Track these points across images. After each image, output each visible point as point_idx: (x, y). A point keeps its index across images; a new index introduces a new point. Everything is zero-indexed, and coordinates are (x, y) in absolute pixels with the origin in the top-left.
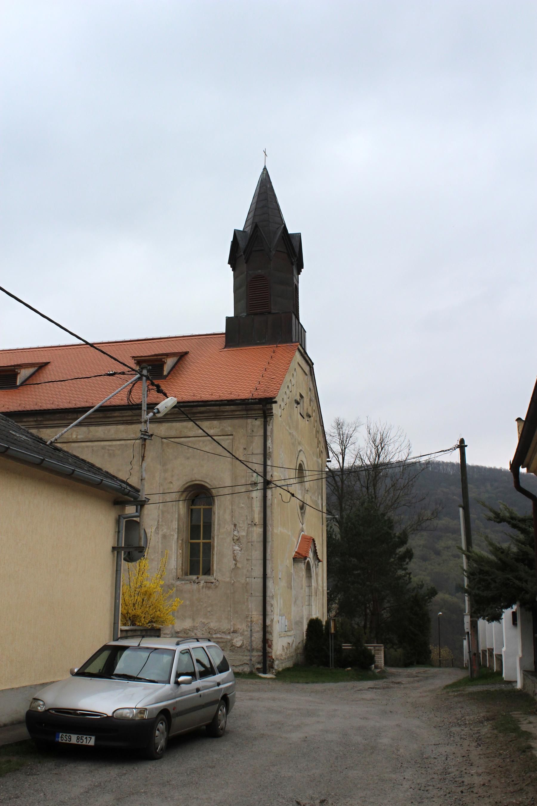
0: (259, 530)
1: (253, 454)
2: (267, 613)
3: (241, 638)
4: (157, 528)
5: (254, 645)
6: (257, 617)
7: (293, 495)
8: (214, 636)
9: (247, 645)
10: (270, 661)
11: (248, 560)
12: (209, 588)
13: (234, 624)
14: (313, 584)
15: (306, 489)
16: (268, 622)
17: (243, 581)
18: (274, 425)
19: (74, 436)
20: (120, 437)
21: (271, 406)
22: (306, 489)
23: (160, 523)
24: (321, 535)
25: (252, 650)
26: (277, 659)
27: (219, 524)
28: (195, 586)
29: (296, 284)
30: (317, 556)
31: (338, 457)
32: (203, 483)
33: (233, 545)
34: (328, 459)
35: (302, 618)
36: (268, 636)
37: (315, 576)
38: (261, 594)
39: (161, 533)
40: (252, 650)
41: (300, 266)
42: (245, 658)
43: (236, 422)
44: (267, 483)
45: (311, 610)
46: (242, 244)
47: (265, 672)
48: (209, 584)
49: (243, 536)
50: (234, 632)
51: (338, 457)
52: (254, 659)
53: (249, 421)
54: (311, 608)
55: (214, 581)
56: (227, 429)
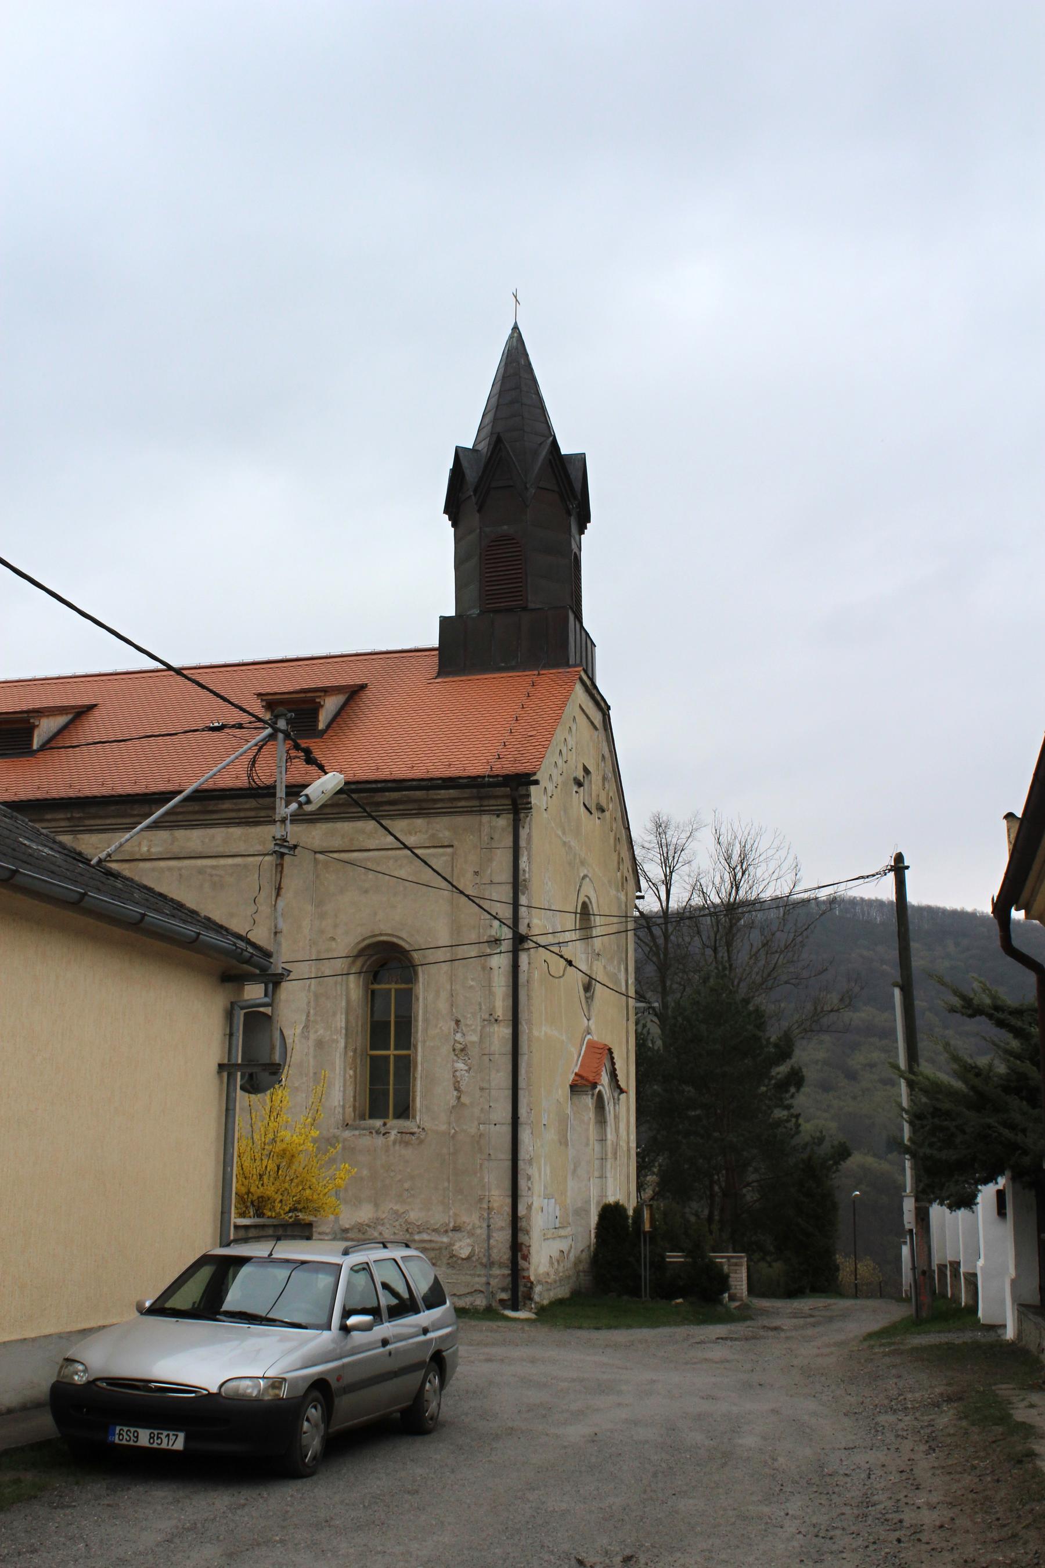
0: (504, 1031)
1: (492, 883)
2: (519, 1192)
3: (468, 1241)
4: (306, 1027)
5: (495, 1255)
6: (500, 1199)
7: (570, 963)
8: (417, 1237)
9: (481, 1255)
10: (525, 1286)
11: (482, 1089)
12: (407, 1144)
13: (455, 1214)
14: (609, 1137)
15: (596, 952)
16: (522, 1211)
17: (473, 1131)
18: (534, 826)
19: (145, 849)
20: (234, 850)
21: (528, 790)
22: (596, 952)
23: (312, 1018)
24: (624, 1040)
25: (491, 1264)
26: (539, 1282)
27: (426, 1020)
28: (380, 1140)
29: (575, 553)
30: (617, 1081)
31: (657, 889)
32: (395, 940)
33: (453, 1061)
34: (638, 894)
35: (588, 1202)
36: (522, 1238)
37: (613, 1120)
38: (507, 1155)
39: (312, 1036)
40: (491, 1264)
41: (584, 518)
42: (477, 1279)
43: (460, 820)
44: (519, 941)
45: (606, 1186)
46: (471, 475)
47: (515, 1308)
48: (407, 1137)
49: (473, 1043)
50: (456, 1229)
51: (657, 889)
52: (494, 1282)
53: (485, 818)
54: (606, 1183)
55: (416, 1130)
56: (441, 835)
